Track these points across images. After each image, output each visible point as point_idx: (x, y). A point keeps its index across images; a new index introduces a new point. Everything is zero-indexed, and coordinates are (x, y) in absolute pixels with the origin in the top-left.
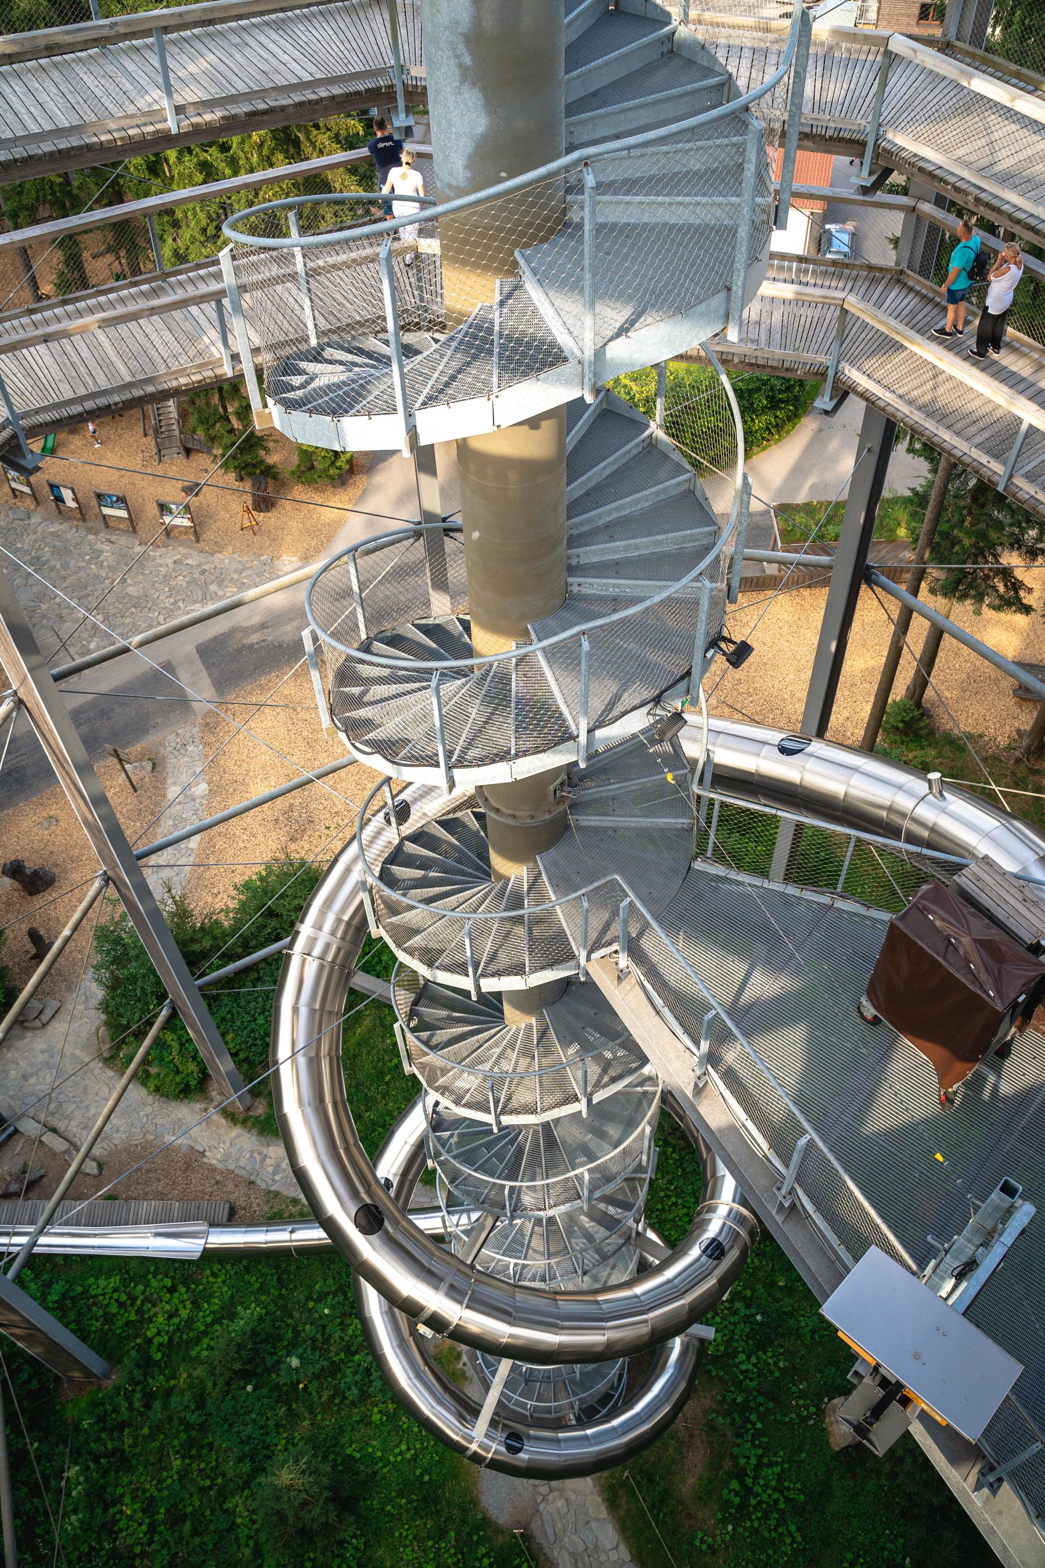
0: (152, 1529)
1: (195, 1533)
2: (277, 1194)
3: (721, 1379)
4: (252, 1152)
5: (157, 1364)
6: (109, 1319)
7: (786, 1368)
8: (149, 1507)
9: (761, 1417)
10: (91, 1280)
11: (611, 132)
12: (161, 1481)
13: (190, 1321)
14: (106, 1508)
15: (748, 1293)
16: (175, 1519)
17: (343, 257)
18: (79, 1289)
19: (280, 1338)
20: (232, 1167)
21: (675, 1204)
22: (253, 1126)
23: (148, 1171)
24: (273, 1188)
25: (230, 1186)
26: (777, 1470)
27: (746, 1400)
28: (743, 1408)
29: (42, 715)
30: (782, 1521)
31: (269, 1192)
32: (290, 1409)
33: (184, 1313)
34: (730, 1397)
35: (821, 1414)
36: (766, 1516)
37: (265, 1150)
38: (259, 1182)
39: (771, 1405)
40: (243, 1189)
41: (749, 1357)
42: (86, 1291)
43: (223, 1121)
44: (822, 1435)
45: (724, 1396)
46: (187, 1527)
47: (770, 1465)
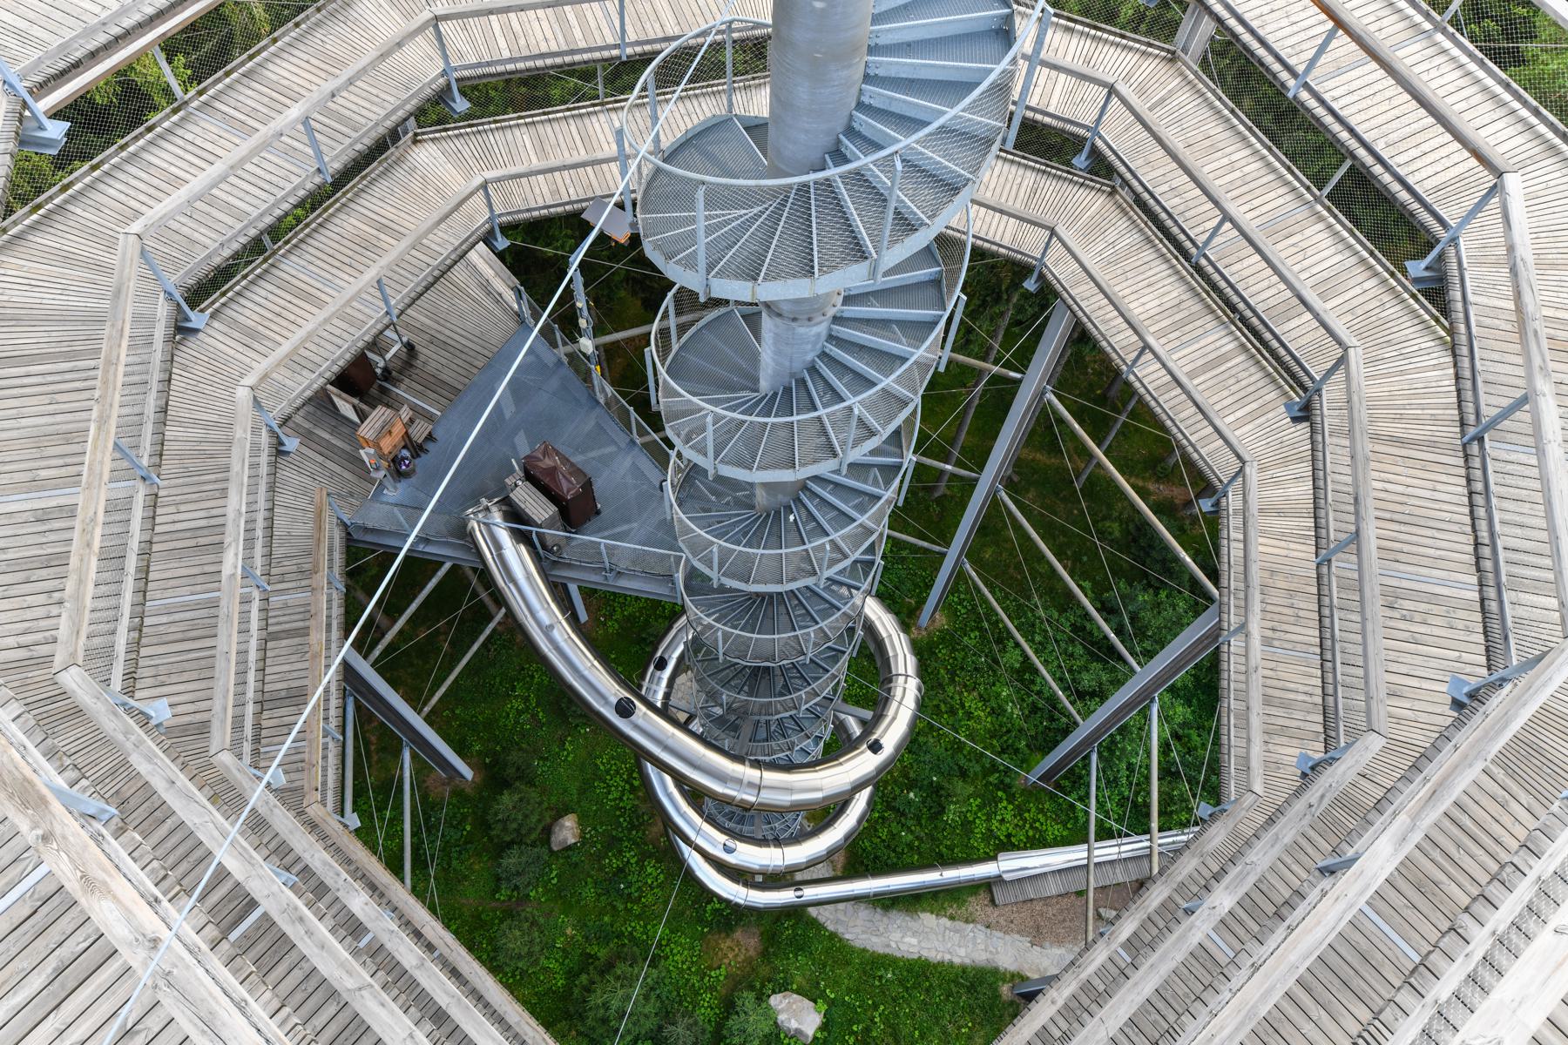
0: (963, 706)
1: (937, 706)
2: (967, 921)
3: (646, 844)
4: (997, 953)
5: (999, 789)
6: (1041, 811)
7: (604, 859)
8: (969, 715)
9: (620, 824)
10: (1065, 833)
11: (1495, 815)
12: (968, 729)
13: (989, 820)
14: (992, 709)
15: (629, 905)
16: (952, 712)
17: (1302, 374)
18: (1069, 826)
19: (928, 819)
20: (1007, 937)
21: (683, 963)
22: (1004, 974)
23: (1064, 920)
24: (971, 925)
25: (1002, 920)
26: (610, 797)
27: (630, 833)
28: (633, 827)
29: (903, 279)
30: (607, 772)
31: (973, 921)
32: (908, 779)
33: (995, 824)
34: (640, 834)
35: (582, 836)
36: (617, 772)
37: (989, 956)
38: (983, 928)
39: (614, 833)
40: (992, 920)
41: (628, 862)
42: (1065, 825)
43: (1029, 975)
44: (582, 821)
45: (644, 834)
46: (943, 707)
47: (615, 799)
